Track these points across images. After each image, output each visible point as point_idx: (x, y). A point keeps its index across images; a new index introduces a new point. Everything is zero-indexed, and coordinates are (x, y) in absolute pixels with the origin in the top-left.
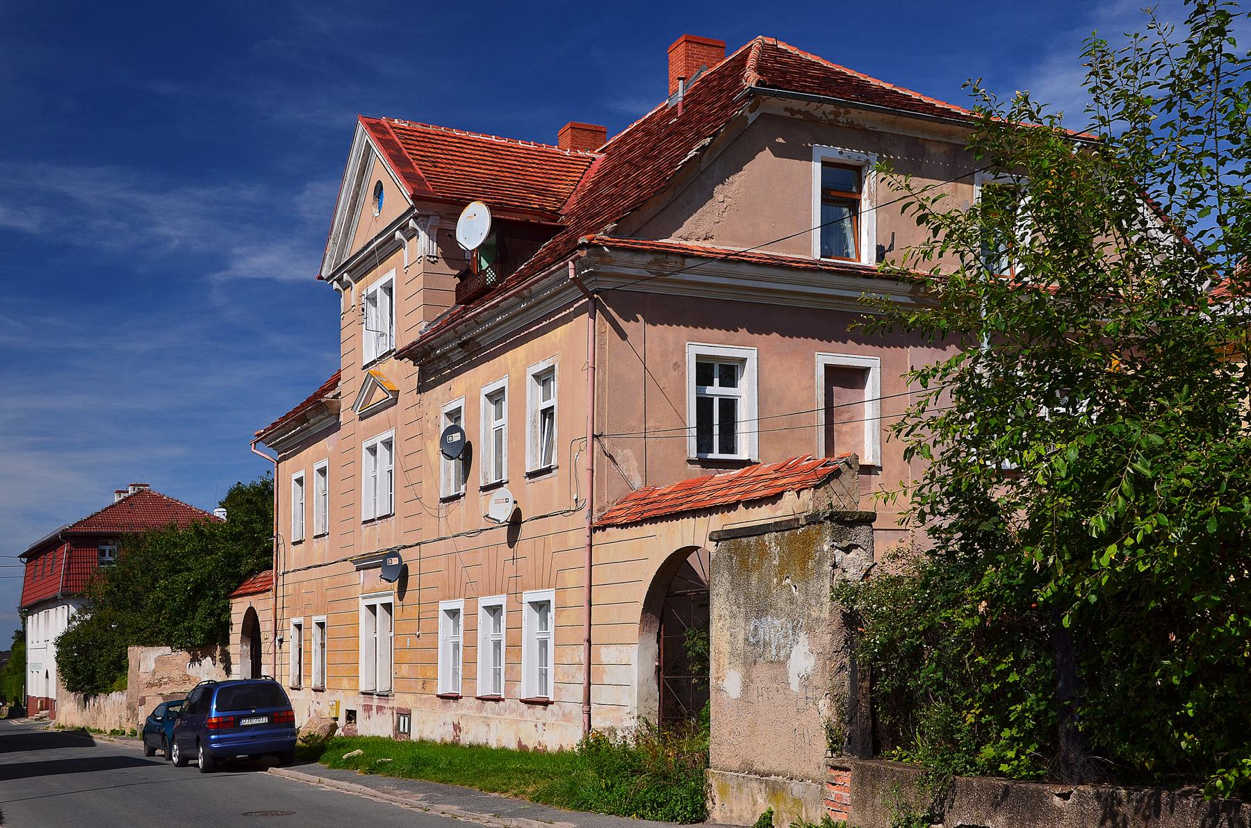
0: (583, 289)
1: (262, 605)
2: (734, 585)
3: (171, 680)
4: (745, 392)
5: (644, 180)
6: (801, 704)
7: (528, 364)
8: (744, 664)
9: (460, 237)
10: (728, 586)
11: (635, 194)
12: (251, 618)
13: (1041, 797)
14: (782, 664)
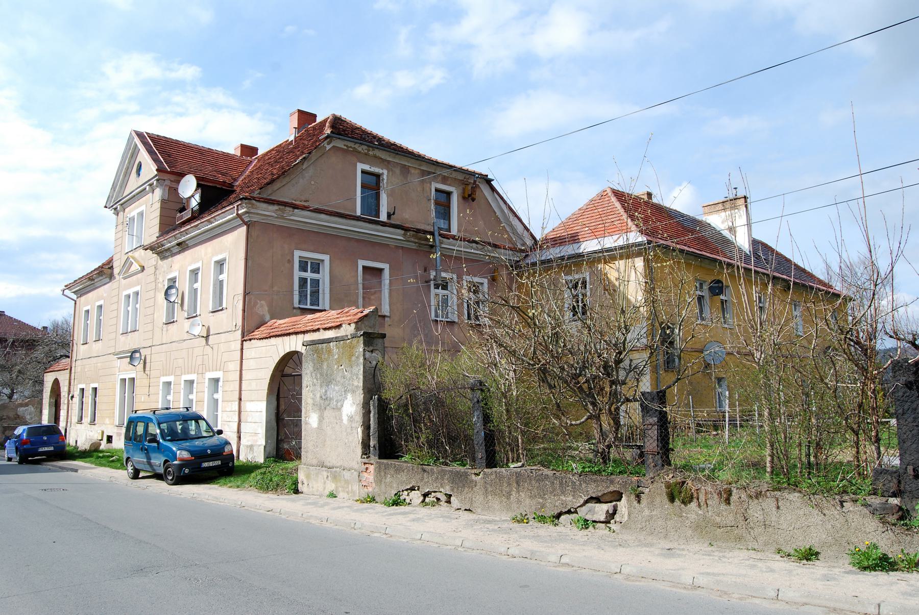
0: (242, 220)
1: (63, 377)
2: (316, 369)
3: (9, 418)
4: (324, 276)
5: (275, 171)
6: (349, 430)
7: (213, 255)
8: (320, 409)
9: (180, 191)
10: (311, 369)
11: (270, 177)
12: (56, 383)
13: (466, 475)
14: (339, 409)
